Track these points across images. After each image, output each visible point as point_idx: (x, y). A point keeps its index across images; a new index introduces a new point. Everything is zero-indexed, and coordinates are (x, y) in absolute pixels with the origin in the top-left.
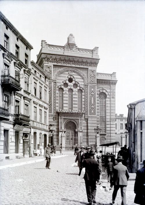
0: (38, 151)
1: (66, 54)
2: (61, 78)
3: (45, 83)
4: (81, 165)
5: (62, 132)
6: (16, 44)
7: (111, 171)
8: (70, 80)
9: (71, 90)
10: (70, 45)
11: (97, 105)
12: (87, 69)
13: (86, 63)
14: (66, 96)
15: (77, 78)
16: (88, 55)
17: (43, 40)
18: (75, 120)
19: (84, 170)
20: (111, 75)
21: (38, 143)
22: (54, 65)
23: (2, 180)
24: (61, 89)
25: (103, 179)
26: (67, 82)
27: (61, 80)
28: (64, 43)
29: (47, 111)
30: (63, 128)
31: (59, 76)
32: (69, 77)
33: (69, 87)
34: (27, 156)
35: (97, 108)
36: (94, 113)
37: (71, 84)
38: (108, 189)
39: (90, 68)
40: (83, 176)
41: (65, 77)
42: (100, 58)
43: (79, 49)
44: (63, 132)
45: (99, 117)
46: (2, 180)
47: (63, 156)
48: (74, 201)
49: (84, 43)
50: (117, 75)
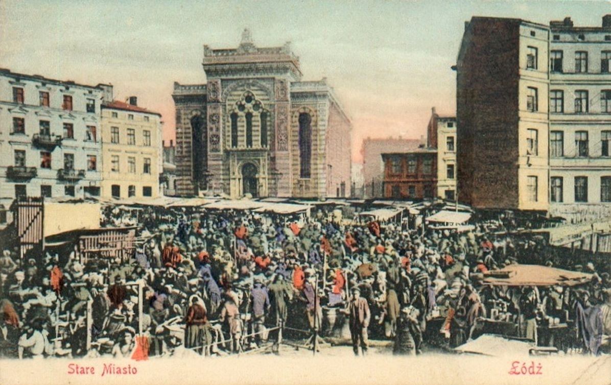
2: (235, 98)
5: (235, 179)
8: (249, 99)
9: (249, 116)
12: (274, 79)
13: (271, 69)
14: (242, 124)
15: (258, 96)
18: (264, 83)
20: (317, 83)
22: (222, 80)
23: (76, 248)
24: (234, 116)
26: (244, 102)
27: (234, 100)
30: (236, 173)
31: (231, 95)
32: (246, 94)
33: (246, 111)
37: (249, 106)
39: (278, 77)
40: (571, 20)
41: (239, 95)
44: (237, 180)
46: (76, 248)
48: (126, 205)
49: (266, 37)
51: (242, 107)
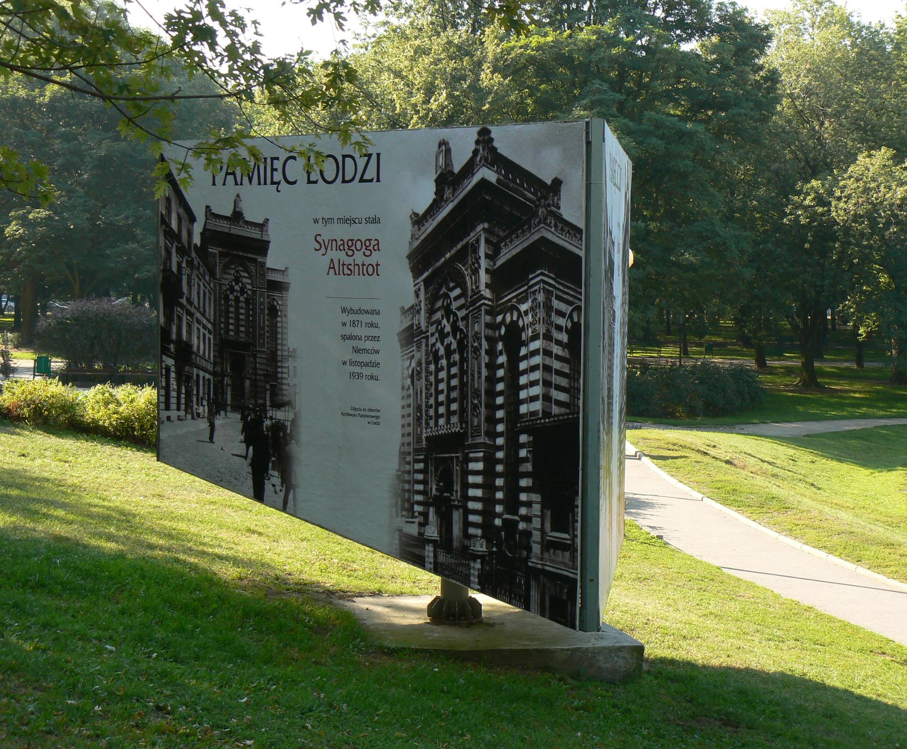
0: (201, 410)
1: (233, 232)
3: (209, 284)
4: (248, 442)
6: (207, 207)
7: (531, 484)
10: (237, 216)
11: (267, 329)
16: (255, 234)
17: (306, 181)
19: (251, 448)
21: (201, 395)
25: (273, 469)
28: (228, 212)
29: (212, 337)
34: (189, 417)
35: (267, 334)
36: (263, 346)
38: (278, 488)
42: (270, 239)
43: (248, 223)
45: (268, 352)
47: (228, 420)
50: (290, 271)
51: (232, 289)
